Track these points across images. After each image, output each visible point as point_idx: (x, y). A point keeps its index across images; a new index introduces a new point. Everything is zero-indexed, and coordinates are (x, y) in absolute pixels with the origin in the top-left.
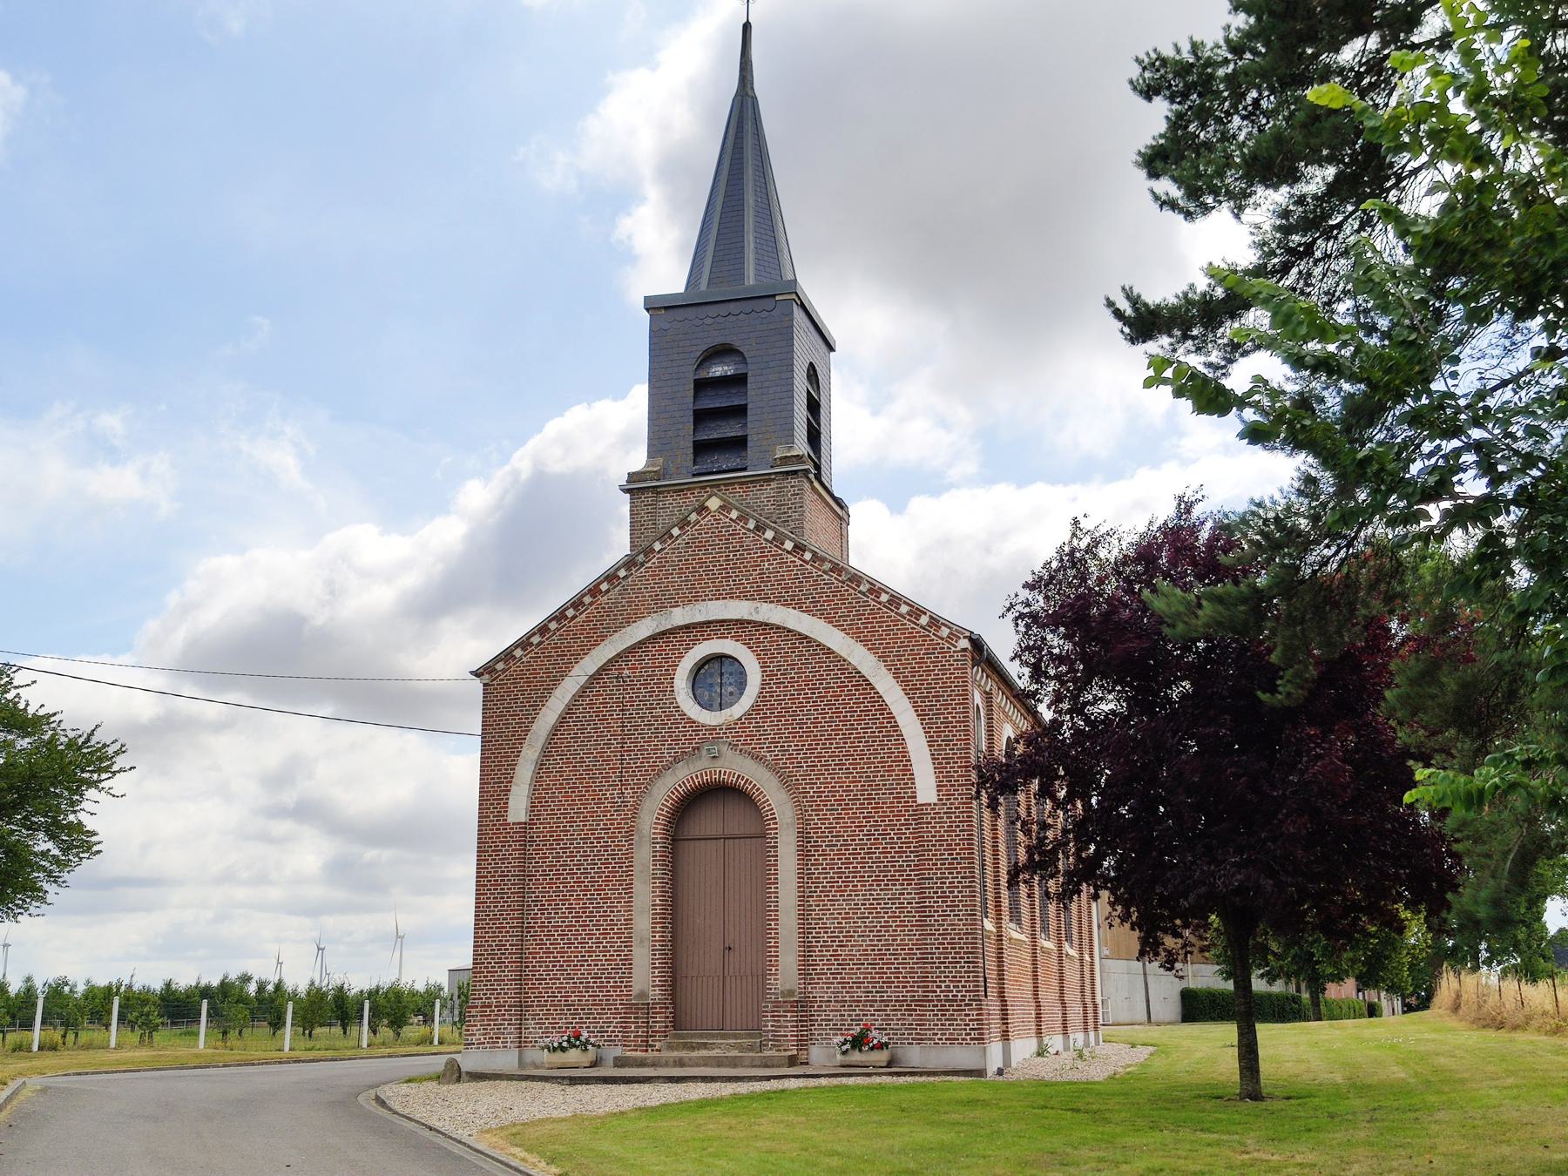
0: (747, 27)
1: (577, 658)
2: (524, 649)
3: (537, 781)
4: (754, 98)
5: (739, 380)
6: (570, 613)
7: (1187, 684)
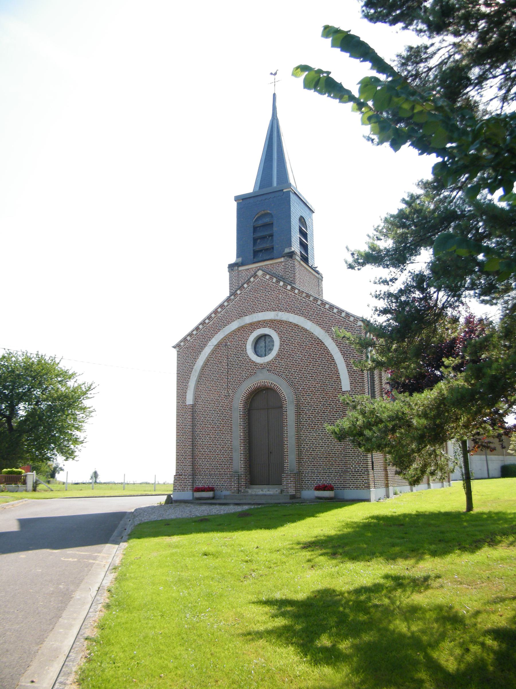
0: (274, 95)
1: (210, 339)
2: (191, 336)
3: (197, 387)
4: (277, 120)
5: (270, 225)
6: (207, 321)
7: (459, 213)
